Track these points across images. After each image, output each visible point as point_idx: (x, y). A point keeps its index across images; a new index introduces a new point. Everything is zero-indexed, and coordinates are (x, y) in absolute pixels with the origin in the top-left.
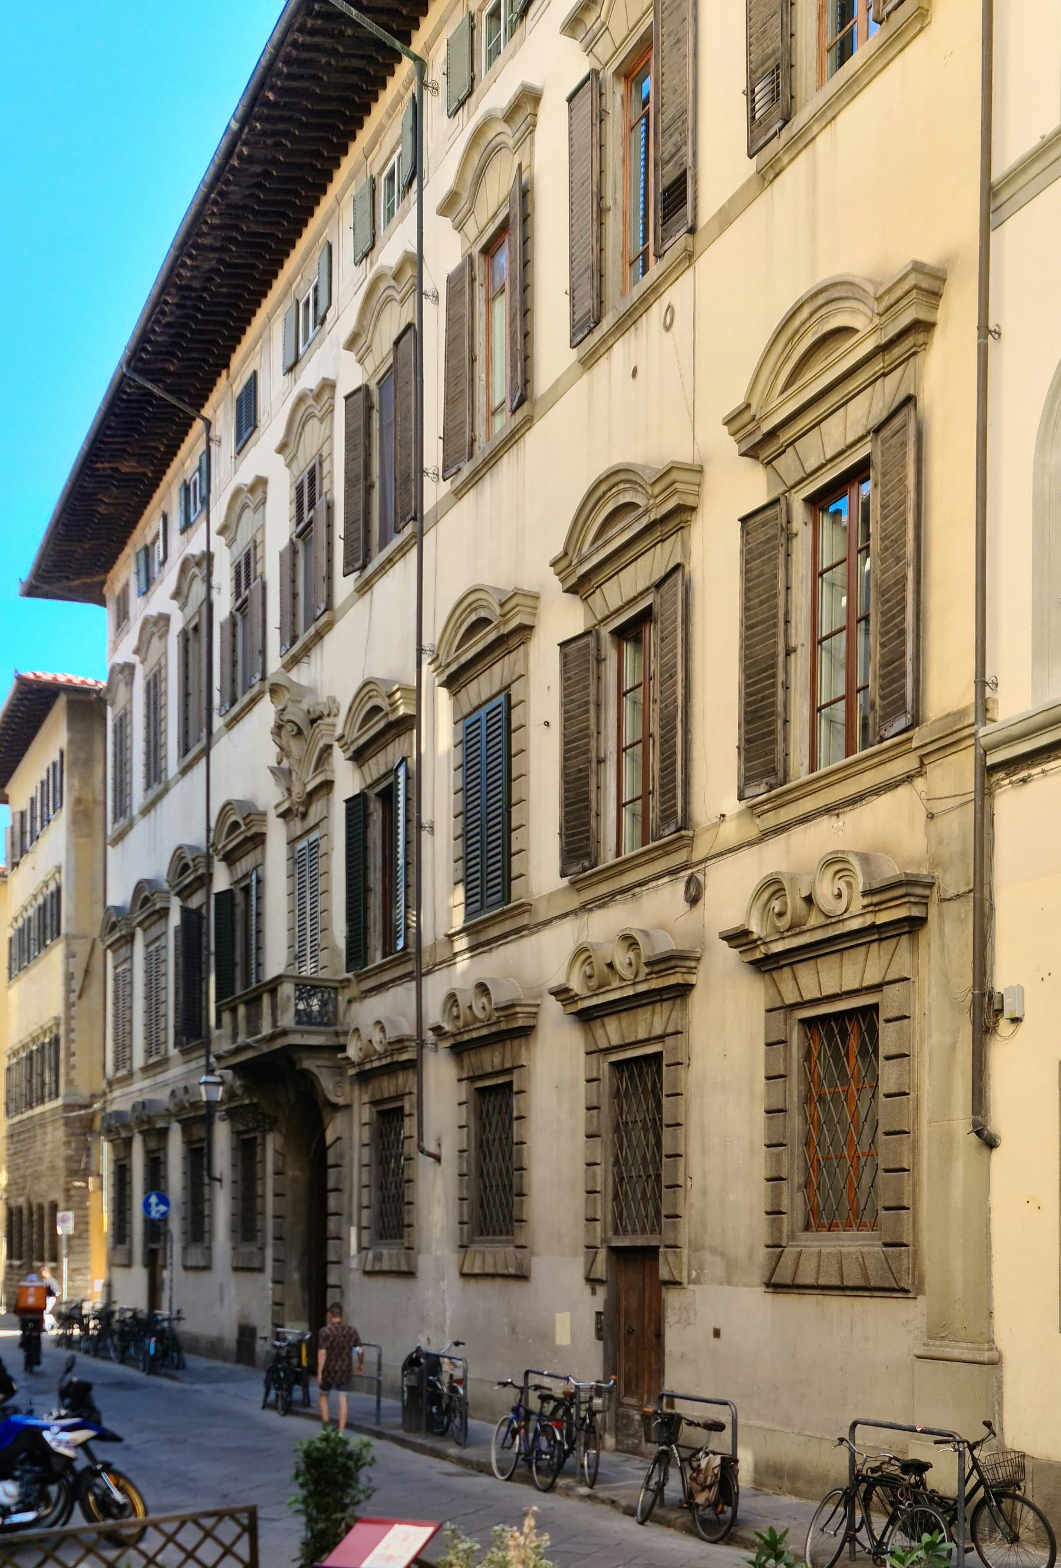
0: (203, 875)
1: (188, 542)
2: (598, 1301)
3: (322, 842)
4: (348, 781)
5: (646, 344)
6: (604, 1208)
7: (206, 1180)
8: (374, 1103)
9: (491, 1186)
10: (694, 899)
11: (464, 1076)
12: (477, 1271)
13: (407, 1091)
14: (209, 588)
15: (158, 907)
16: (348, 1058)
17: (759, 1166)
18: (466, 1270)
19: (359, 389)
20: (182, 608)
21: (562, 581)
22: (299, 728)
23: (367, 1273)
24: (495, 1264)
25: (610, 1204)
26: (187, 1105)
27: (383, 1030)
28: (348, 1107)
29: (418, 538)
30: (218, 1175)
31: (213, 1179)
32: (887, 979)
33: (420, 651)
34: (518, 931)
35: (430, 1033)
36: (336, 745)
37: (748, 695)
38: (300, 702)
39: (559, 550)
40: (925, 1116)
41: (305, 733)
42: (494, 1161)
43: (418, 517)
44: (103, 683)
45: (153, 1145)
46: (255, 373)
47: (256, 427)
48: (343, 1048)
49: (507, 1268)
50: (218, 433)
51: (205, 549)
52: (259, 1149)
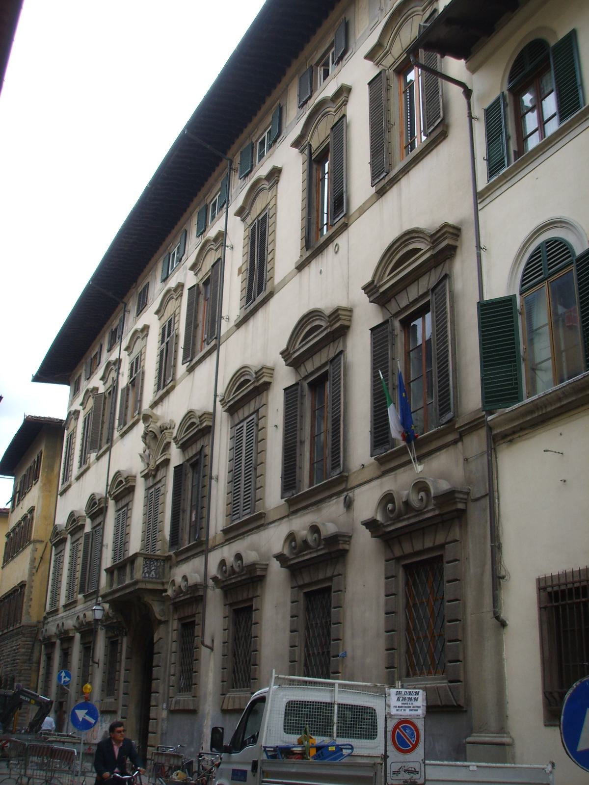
0: (103, 507)
1: (110, 355)
3: (162, 489)
4: (176, 457)
5: (328, 260)
7: (91, 663)
8: (179, 619)
9: (239, 661)
11: (227, 603)
13: (197, 612)
14: (118, 374)
15: (79, 524)
18: (225, 707)
19: (194, 286)
20: (104, 384)
22: (155, 434)
24: (240, 704)
26: (84, 623)
28: (166, 622)
29: (216, 348)
30: (97, 661)
32: (447, 541)
33: (216, 396)
34: (258, 527)
35: (211, 580)
36: (172, 441)
37: (375, 407)
38: (157, 422)
39: (284, 347)
40: (469, 610)
41: (158, 436)
42: (241, 647)
43: (218, 338)
44: (64, 418)
45: (65, 646)
46: (148, 282)
47: (146, 304)
48: (166, 591)
50: (129, 308)
51: (118, 357)
52: (119, 646)
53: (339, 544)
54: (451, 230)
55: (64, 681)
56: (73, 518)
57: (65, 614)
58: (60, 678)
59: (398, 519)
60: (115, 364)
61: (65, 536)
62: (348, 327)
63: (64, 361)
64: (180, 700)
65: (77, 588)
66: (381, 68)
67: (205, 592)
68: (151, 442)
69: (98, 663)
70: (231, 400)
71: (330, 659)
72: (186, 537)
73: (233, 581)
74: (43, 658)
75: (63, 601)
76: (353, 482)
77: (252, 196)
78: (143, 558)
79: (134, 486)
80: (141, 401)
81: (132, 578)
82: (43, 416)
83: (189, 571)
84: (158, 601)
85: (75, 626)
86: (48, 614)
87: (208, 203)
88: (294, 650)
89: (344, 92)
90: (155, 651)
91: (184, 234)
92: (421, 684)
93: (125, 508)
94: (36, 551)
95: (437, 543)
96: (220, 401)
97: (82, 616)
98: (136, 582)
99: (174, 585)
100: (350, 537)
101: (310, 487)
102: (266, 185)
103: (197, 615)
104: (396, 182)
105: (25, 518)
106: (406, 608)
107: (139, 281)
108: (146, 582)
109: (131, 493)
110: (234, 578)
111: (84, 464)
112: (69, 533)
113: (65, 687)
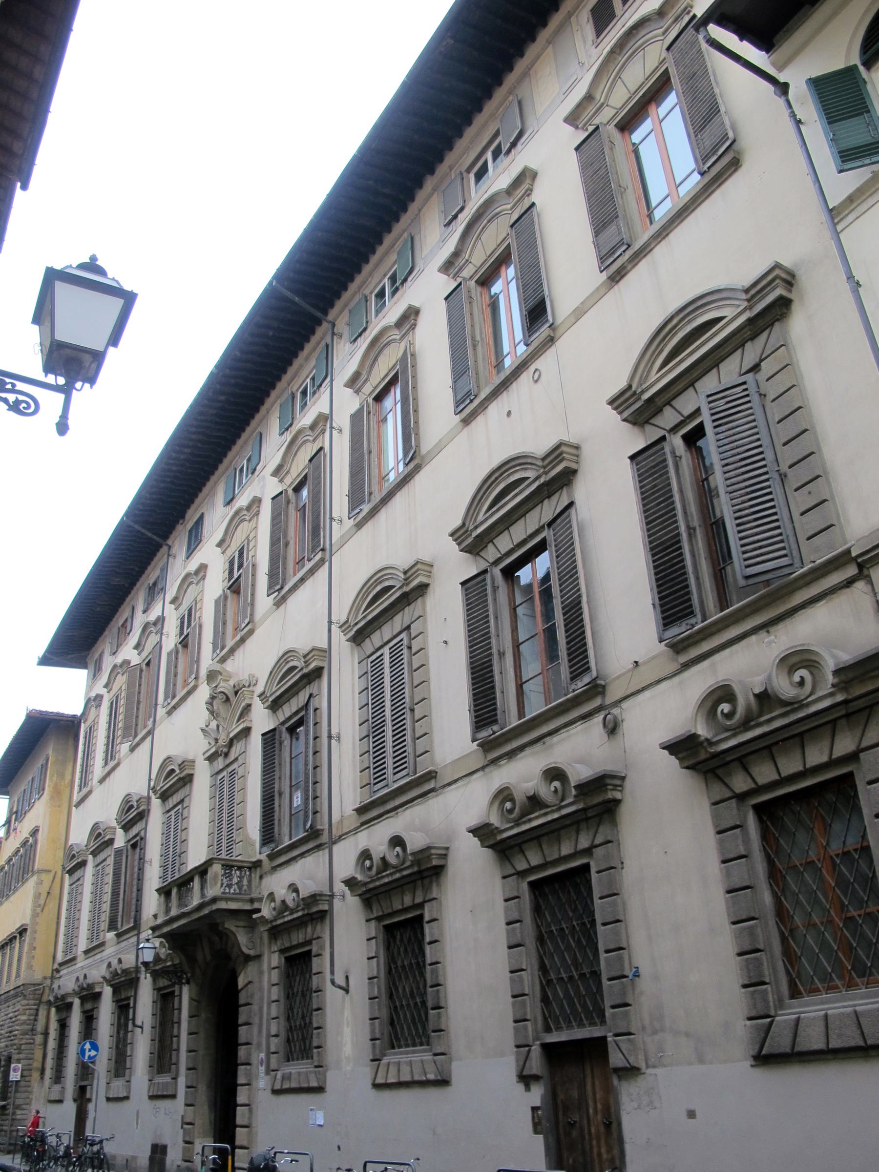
0: (144, 811)
2: (536, 1095)
3: (241, 772)
4: (262, 720)
6: (533, 1008)
8: (282, 951)
10: (613, 729)
12: (392, 1080)
13: (315, 936)
15: (106, 839)
16: (263, 917)
17: (726, 942)
18: (380, 1080)
21: (459, 544)
23: (275, 1092)
25: (538, 1004)
26: (119, 972)
27: (296, 891)
28: (258, 957)
31: (134, 1025)
33: (330, 622)
45: (88, 1006)
47: (201, 540)
48: (258, 911)
49: (425, 1074)
52: (176, 1000)
53: (607, 789)
54: (784, 276)
55: (89, 1056)
56: (96, 832)
57: (87, 962)
58: (82, 1052)
59: (746, 724)
60: (155, 624)
61: (85, 858)
62: (574, 472)
63: (80, 638)
64: (291, 1073)
65: (104, 925)
66: (459, 280)
67: (331, 905)
68: (221, 707)
69: (141, 1027)
70: (361, 620)
71: (427, 1014)
72: (285, 830)
73: (386, 880)
74: (54, 1026)
75: (83, 944)
76: (613, 694)
77: (372, 356)
78: (220, 866)
79: (192, 775)
80: (198, 662)
81: (203, 895)
82: (50, 710)
83: (304, 875)
84: (244, 927)
85: (104, 978)
86: (61, 965)
87: (294, 390)
88: (521, 977)
89: (323, 421)
90: (242, 1001)
91: (258, 438)
92: (844, 1007)
93: (180, 806)
94: (41, 883)
95: (838, 752)
96: (259, 696)
97: (115, 962)
98: (214, 900)
99: (273, 900)
100: (623, 778)
101: (520, 719)
102: (396, 334)
103: (314, 942)
104: (645, 256)
105: (25, 843)
106: (769, 878)
107: (187, 516)
108: (227, 900)
109: (188, 785)
110: (387, 875)
111: (111, 759)
112: (92, 853)
113: (90, 1065)
